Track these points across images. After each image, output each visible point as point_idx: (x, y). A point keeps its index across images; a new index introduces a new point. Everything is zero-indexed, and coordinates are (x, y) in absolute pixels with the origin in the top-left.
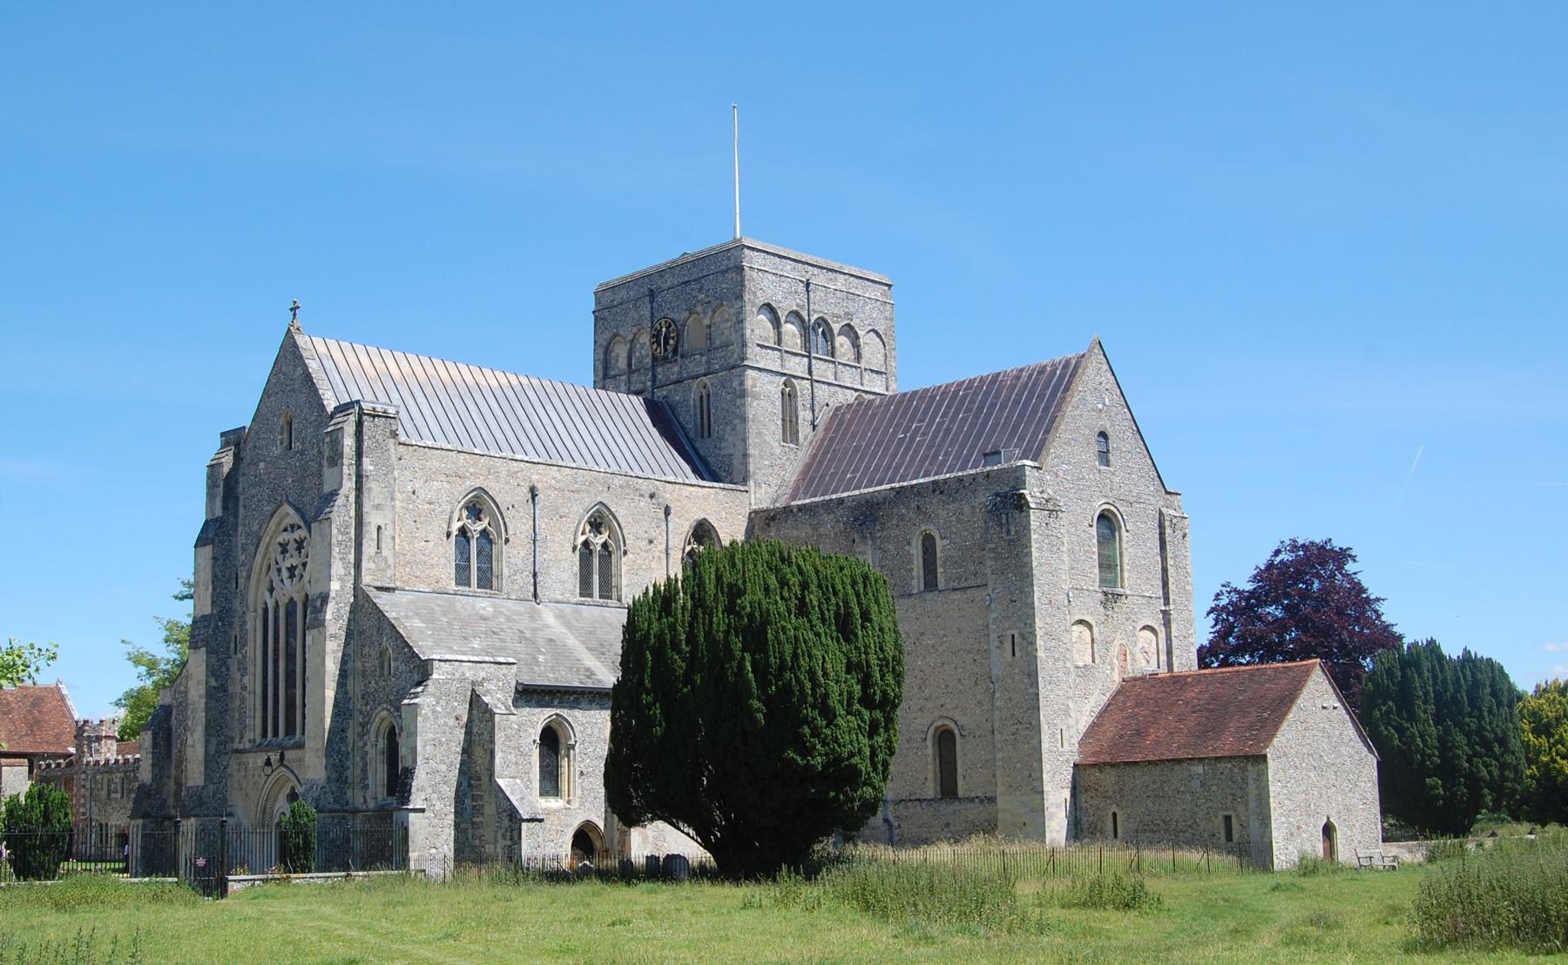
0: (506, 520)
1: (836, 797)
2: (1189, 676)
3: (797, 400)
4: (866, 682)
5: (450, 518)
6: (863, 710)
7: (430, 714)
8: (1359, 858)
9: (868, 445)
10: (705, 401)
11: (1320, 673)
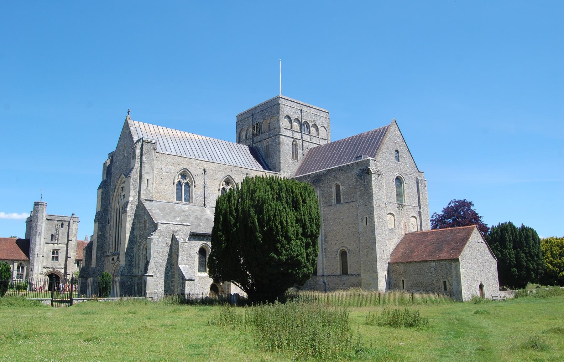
0: (195, 179)
1: (292, 272)
2: (429, 232)
3: (297, 146)
4: (304, 227)
5: (174, 178)
6: (303, 238)
7: (156, 242)
8: (492, 297)
9: (320, 159)
10: (268, 147)
11: (477, 230)
